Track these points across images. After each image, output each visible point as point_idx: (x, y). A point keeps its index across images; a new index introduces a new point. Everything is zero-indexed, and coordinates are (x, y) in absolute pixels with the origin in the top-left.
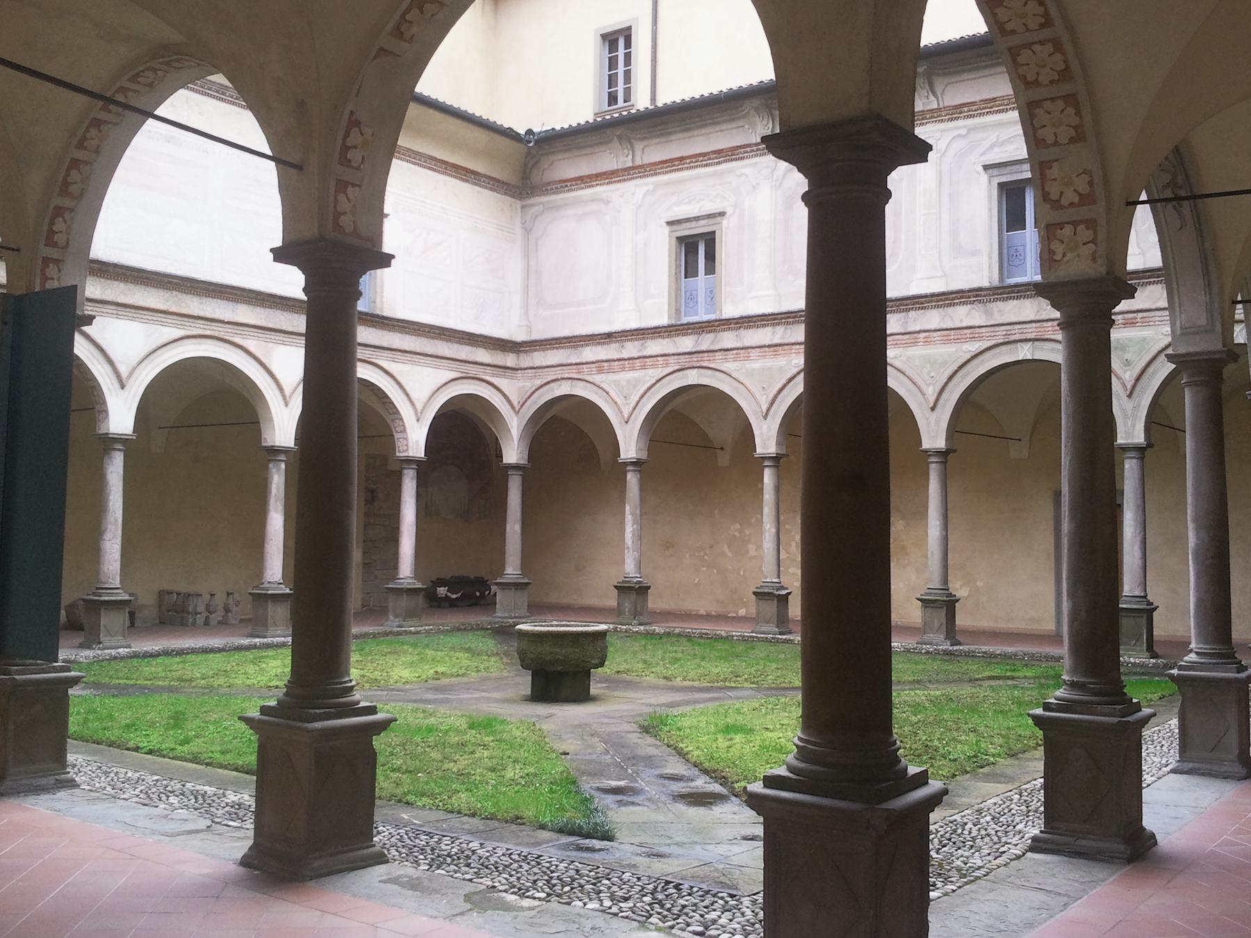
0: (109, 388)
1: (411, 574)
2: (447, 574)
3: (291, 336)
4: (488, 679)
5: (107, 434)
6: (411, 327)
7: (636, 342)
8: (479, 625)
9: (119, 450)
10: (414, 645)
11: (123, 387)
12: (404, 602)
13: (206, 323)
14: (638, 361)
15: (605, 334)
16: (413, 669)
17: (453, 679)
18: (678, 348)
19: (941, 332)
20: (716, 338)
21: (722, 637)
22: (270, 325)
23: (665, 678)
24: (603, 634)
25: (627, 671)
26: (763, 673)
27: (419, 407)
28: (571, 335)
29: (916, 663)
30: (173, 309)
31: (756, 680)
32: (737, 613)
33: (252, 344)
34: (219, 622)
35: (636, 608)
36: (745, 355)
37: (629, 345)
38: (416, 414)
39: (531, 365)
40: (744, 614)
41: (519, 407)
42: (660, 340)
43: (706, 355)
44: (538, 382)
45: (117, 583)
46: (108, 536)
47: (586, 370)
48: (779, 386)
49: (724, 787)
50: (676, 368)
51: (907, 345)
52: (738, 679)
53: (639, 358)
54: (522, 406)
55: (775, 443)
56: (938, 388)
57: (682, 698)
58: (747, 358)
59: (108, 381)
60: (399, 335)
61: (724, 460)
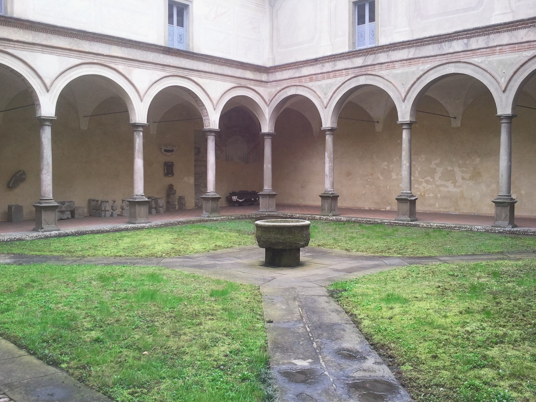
0: (40, 92)
1: (213, 190)
2: (237, 190)
3: (142, 63)
4: (245, 249)
5: (40, 117)
6: (209, 58)
7: (331, 63)
8: (249, 216)
9: (48, 125)
10: (210, 228)
11: (48, 91)
12: (210, 204)
13: (94, 56)
14: (331, 73)
15: (313, 59)
16: (202, 244)
17: (225, 250)
18: (354, 64)
19: (509, 46)
20: (375, 57)
21: (378, 223)
22: (130, 57)
23: (346, 250)
24: (307, 227)
25: (324, 245)
26: (405, 247)
27: (215, 102)
28: (295, 61)
29: (496, 240)
30: (75, 48)
31: (401, 251)
32: (386, 208)
33: (120, 68)
34: (118, 215)
35: (331, 207)
36: (392, 66)
37: (327, 65)
38: (214, 106)
39: (275, 79)
40: (389, 209)
41: (269, 102)
42: (344, 61)
43: (370, 67)
44: (279, 89)
45: (51, 197)
46: (44, 171)
47: (304, 80)
48: (412, 82)
49: (391, 369)
50: (353, 76)
51: (488, 55)
52: (390, 251)
53: (332, 72)
54: (271, 102)
55: (409, 116)
56: (508, 79)
57: (355, 265)
58: (394, 68)
59: (39, 87)
60: (203, 63)
61: (379, 128)
